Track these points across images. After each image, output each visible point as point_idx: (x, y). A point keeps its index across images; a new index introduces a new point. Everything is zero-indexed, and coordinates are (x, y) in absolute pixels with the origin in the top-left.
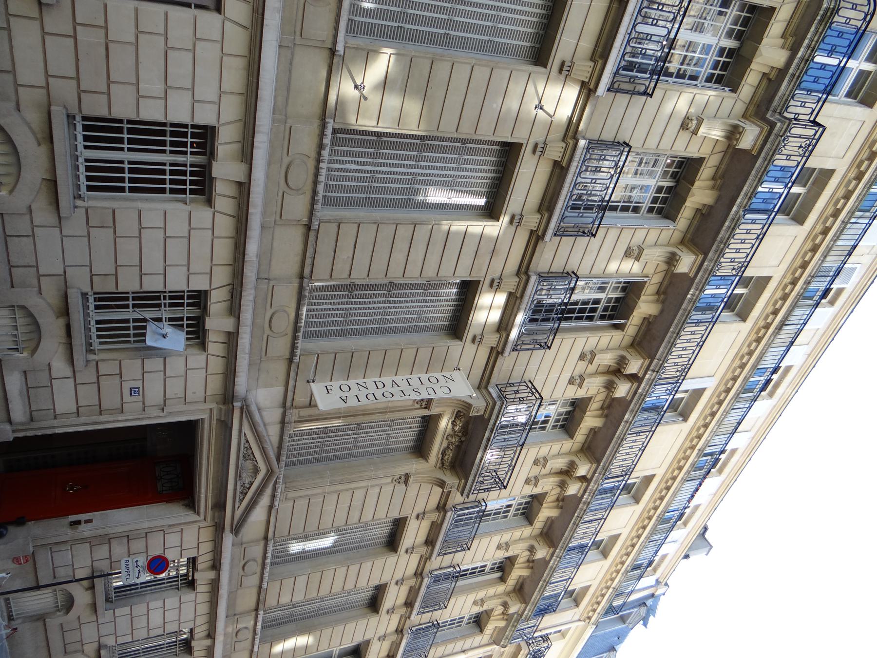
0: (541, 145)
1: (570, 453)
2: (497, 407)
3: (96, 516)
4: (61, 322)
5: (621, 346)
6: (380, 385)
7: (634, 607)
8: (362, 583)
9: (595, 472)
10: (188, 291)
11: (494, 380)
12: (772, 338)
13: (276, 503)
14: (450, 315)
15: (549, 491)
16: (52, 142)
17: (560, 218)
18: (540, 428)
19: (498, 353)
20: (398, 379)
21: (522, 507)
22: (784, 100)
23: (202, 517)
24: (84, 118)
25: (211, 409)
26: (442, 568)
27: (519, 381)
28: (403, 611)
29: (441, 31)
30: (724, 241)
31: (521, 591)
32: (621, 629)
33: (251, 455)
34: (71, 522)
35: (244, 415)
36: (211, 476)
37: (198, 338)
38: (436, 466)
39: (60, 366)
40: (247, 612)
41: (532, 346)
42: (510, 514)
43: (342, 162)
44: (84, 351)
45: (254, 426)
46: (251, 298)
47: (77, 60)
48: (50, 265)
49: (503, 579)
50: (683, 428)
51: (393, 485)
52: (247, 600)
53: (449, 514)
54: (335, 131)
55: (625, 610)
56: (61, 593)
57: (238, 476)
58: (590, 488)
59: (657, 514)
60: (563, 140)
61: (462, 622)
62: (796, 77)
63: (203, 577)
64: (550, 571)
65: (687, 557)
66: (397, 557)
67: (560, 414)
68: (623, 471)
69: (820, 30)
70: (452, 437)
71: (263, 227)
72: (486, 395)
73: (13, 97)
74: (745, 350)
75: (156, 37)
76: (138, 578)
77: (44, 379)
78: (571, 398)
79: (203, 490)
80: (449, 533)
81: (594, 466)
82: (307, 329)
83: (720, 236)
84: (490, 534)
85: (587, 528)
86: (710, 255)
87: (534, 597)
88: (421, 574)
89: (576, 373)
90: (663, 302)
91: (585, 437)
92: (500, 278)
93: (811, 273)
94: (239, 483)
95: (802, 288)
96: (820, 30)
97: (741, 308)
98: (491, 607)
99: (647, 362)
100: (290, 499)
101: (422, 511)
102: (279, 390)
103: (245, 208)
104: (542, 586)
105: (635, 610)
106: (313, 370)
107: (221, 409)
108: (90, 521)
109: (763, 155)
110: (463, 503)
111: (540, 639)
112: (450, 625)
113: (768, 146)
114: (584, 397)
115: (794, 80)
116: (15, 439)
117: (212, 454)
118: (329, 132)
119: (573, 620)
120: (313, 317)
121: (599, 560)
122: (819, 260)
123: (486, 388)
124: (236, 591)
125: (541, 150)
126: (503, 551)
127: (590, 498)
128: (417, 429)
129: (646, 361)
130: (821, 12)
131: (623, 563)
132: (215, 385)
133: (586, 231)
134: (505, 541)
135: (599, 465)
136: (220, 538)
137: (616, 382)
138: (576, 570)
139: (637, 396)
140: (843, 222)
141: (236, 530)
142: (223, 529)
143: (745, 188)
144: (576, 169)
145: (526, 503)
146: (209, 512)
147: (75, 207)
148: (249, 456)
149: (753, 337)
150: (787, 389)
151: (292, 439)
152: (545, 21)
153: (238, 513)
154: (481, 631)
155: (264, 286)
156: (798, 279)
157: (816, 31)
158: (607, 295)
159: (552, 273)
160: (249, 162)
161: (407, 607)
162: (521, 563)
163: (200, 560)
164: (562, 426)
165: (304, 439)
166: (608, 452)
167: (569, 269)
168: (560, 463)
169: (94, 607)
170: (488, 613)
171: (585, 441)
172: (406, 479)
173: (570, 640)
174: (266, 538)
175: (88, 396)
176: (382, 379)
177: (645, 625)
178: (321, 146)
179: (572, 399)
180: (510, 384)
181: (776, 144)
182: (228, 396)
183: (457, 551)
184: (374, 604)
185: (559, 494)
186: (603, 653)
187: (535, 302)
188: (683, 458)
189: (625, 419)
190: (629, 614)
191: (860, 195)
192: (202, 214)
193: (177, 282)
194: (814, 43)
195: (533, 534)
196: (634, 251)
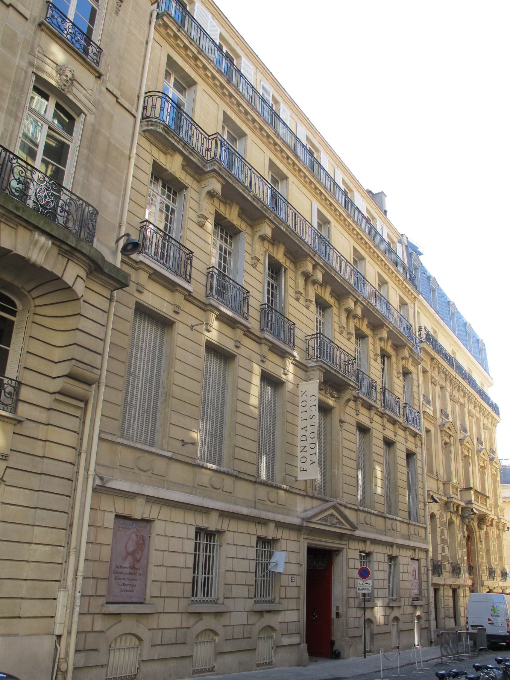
1: (253, 237)
2: (323, 365)
3: (334, 605)
4: (265, 615)
5: (294, 271)
6: (304, 438)
7: (411, 261)
8: (353, 438)
9: (354, 296)
10: (257, 547)
12: (301, 162)
14: (154, 327)
15: (215, 208)
16: (120, 614)
17: (236, 313)
18: (171, 214)
19: (249, 331)
20: (301, 426)
22: (200, 160)
23: (345, 547)
24: (193, 596)
25: (304, 538)
27: (305, 344)
28: (373, 412)
30: (263, 206)
31: (398, 346)
32: (420, 271)
34: (337, 617)
35: (311, 521)
36: (330, 540)
37: (270, 542)
38: (337, 402)
39: (280, 617)
40: (409, 529)
41: (189, 266)
42: (228, 249)
44: (272, 604)
46: (264, 513)
47: (173, 597)
48: (174, 621)
49: (389, 357)
50: (334, 225)
52: (379, 522)
53: (361, 395)
56: (261, 634)
57: (333, 526)
58: (361, 300)
59: (373, 248)
62: (192, 152)
63: (369, 548)
64: (394, 329)
65: (385, 212)
67: (163, 193)
68: (315, 237)
69: (173, 135)
71: (235, 504)
73: (185, 630)
74: (302, 180)
76: (369, 584)
77: (230, 629)
78: (150, 179)
79: (335, 545)
80: (234, 309)
81: (351, 296)
83: (260, 208)
84: (369, 365)
85: (300, 228)
86: (267, 215)
87: (404, 341)
88: (382, 414)
89: (304, 303)
90: (279, 242)
91: (287, 260)
92: (261, 356)
93: (273, 133)
94: (337, 525)
95: (280, 140)
96: (173, 135)
97: (185, 83)
99: (309, 259)
100: (343, 495)
102: (299, 499)
104: (400, 335)
105: (413, 261)
106: (291, 477)
107: (304, 533)
108: (338, 608)
109: (227, 178)
113: (223, 175)
114: (152, 166)
115: (192, 152)
116: (306, 643)
117: (321, 539)
119: (413, 308)
120: (215, 459)
121: (287, 184)
122: (268, 127)
123: (307, 367)
127: (284, 224)
128: (213, 357)
130: (164, 133)
131: (393, 272)
132: (293, 535)
135: (351, 294)
138: (335, 250)
139: (324, 267)
140: (252, 109)
142: (352, 535)
143: (241, 191)
145: (222, 232)
146: (344, 542)
147: (223, 604)
148: (325, 519)
149: (297, 174)
150: (316, 139)
152: (143, 316)
153: (348, 527)
154: (411, 373)
155: (258, 505)
156: (238, 102)
157: (173, 137)
160: (135, 495)
161: (371, 409)
164: (175, 194)
166: (347, 288)
168: (301, 282)
169: (218, 614)
170: (404, 368)
171: (334, 297)
172: (342, 422)
173: (438, 329)
174: (356, 510)
175: (292, 604)
176: (300, 436)
177: (421, 254)
179: (152, 178)
181: (224, 170)
182: (298, 529)
184: (363, 430)
187: (219, 298)
188: (349, 226)
189: (334, 275)
190: (414, 265)
191: (240, 97)
192: (228, 537)
194: (178, 139)
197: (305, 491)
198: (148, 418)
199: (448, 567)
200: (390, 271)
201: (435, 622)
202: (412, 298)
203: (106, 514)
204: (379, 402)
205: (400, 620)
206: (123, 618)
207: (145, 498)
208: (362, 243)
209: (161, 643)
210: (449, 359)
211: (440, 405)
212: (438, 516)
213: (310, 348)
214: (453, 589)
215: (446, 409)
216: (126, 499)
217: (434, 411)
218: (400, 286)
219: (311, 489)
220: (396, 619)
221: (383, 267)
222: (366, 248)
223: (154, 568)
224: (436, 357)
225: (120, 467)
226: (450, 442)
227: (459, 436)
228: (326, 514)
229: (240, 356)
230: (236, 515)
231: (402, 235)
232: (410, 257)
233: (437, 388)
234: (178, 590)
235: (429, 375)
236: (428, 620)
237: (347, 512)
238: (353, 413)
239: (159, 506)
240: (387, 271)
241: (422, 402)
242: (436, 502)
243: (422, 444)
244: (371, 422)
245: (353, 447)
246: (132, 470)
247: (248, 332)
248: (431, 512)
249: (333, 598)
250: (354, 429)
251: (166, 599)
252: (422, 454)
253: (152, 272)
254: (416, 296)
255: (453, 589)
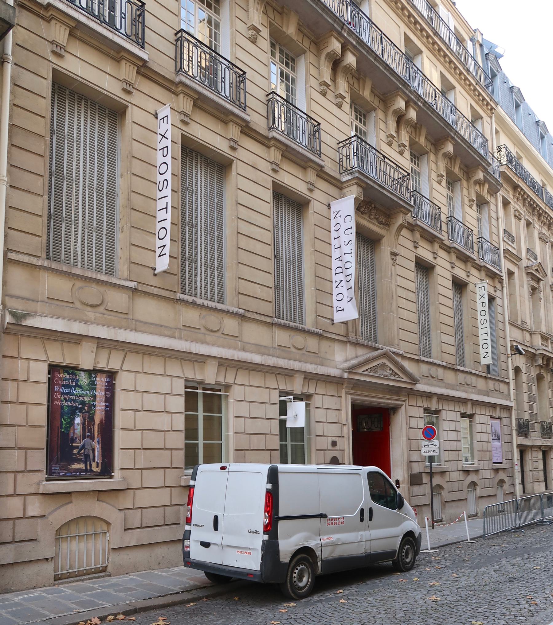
0: (183, 117)
6: (340, 270)
8: (412, 275)
9: (405, 93)
11: (337, 175)
13: (401, 352)
21: (413, 159)
26: (448, 231)
27: (338, 153)
29: (105, 198)
33: (375, 368)
35: (353, 371)
38: (387, 230)
43: (196, 287)
45: (360, 365)
51: (396, 265)
54: (184, 292)
55: (489, 74)
57: (386, 378)
60: (177, 95)
61: (415, 171)
63: (434, 405)
66: (438, 266)
70: (371, 215)
71: (244, 350)
72: (349, 183)
75: (137, 417)
76: (436, 446)
79: (390, 401)
82: (216, 301)
98: (444, 169)
101: (413, 243)
102: (337, 347)
103: (233, 362)
110: (448, 233)
111: (498, 154)
112: (416, 183)
117: (371, 394)
118: (185, 297)
124: (445, 383)
125: (59, 48)
126: (344, 103)
129: (411, 104)
133: (138, 13)
134: (436, 176)
136: (418, 392)
137: (396, 108)
141: (415, 381)
144: (201, 86)
146: (401, 398)
148: (374, 369)
151: (281, 316)
153: (406, 379)
158: (277, 63)
159: (176, 58)
160: (80, 338)
162: (480, 190)
163: (425, 406)
165: (283, 307)
167: (172, 38)
172: (394, 254)
174: (418, 361)
176: (334, 268)
178: (194, 304)
180: (340, 162)
183: (319, 138)
185: (353, 76)
186: (513, 98)
193: (179, 403)
195: (434, 152)
196: (324, 89)
197: (346, 336)
198: (100, 239)
199: (538, 428)
200: (458, 71)
201: (522, 486)
202: (488, 109)
203: (32, 363)
204: (476, 254)
205: (478, 485)
206: (73, 497)
207: (96, 341)
208: (416, 29)
209: (141, 524)
210: (538, 189)
211: (526, 243)
212: (524, 369)
213: (344, 158)
214: (543, 451)
215: (534, 248)
216: (65, 345)
217: (519, 250)
218: (472, 93)
219: (354, 334)
220: (473, 484)
221: (447, 65)
222: (423, 36)
223: (121, 432)
224: (520, 184)
225: (50, 301)
226: (539, 287)
227: (550, 281)
228: (375, 364)
229: (238, 161)
230: (245, 364)
231: (475, 31)
232: (485, 60)
233: (523, 223)
234: (164, 459)
235: (512, 207)
236: (513, 485)
237: (406, 364)
238: (410, 245)
239: (123, 353)
240: (452, 71)
241: (503, 238)
242: (520, 353)
243: (502, 287)
244: (435, 258)
245: (412, 286)
246: (71, 305)
247: (321, 173)
248: (515, 366)
249: (391, 462)
250: (412, 265)
251: (144, 471)
252: (502, 299)
253: (141, 65)
254: (494, 106)
255: (543, 451)
